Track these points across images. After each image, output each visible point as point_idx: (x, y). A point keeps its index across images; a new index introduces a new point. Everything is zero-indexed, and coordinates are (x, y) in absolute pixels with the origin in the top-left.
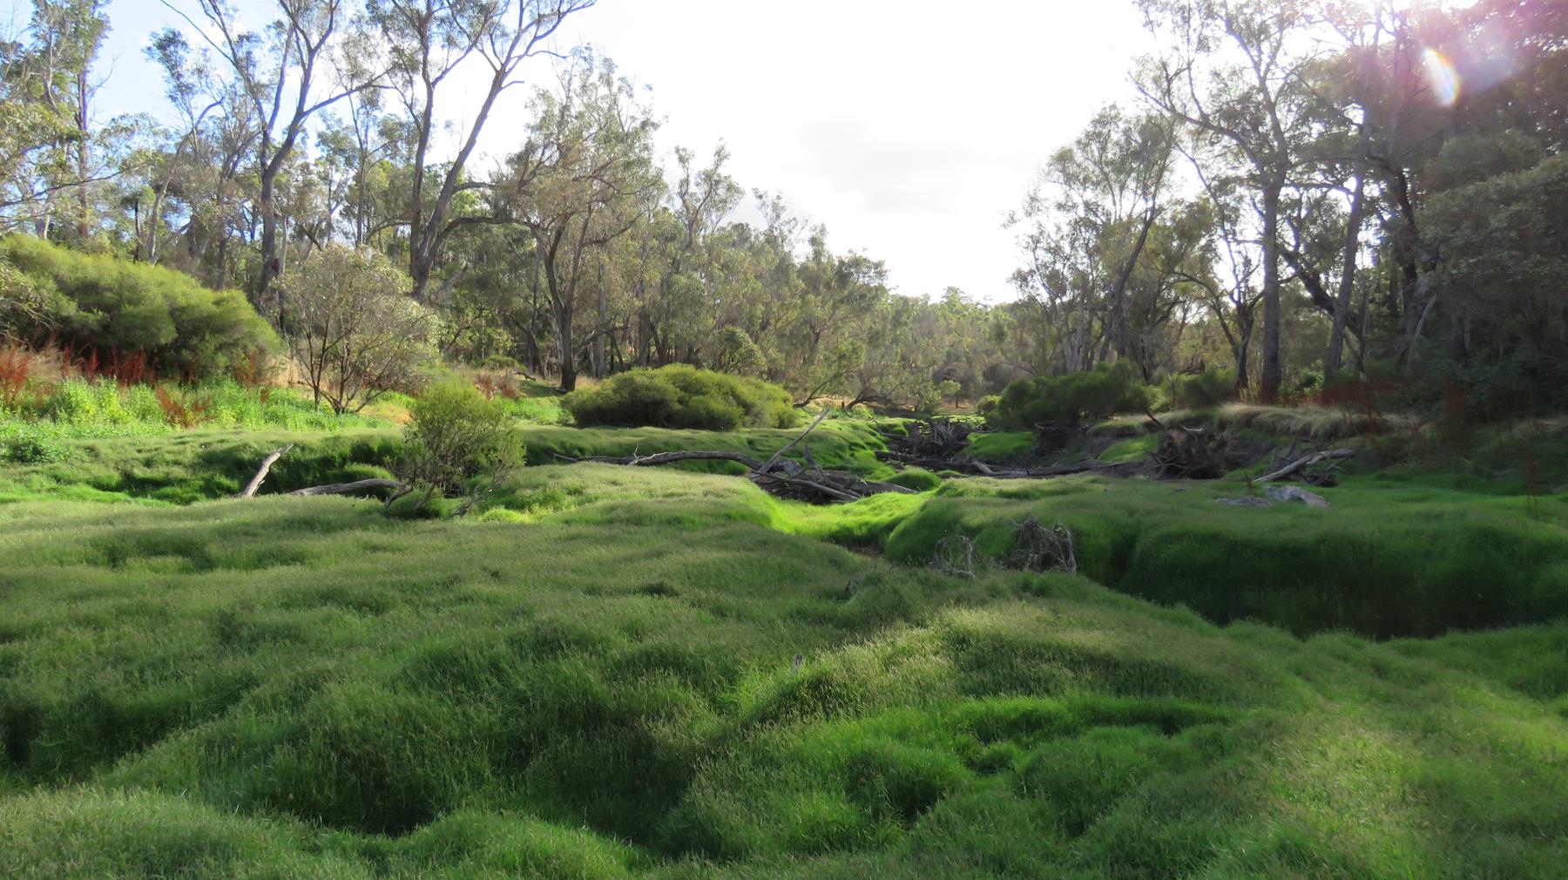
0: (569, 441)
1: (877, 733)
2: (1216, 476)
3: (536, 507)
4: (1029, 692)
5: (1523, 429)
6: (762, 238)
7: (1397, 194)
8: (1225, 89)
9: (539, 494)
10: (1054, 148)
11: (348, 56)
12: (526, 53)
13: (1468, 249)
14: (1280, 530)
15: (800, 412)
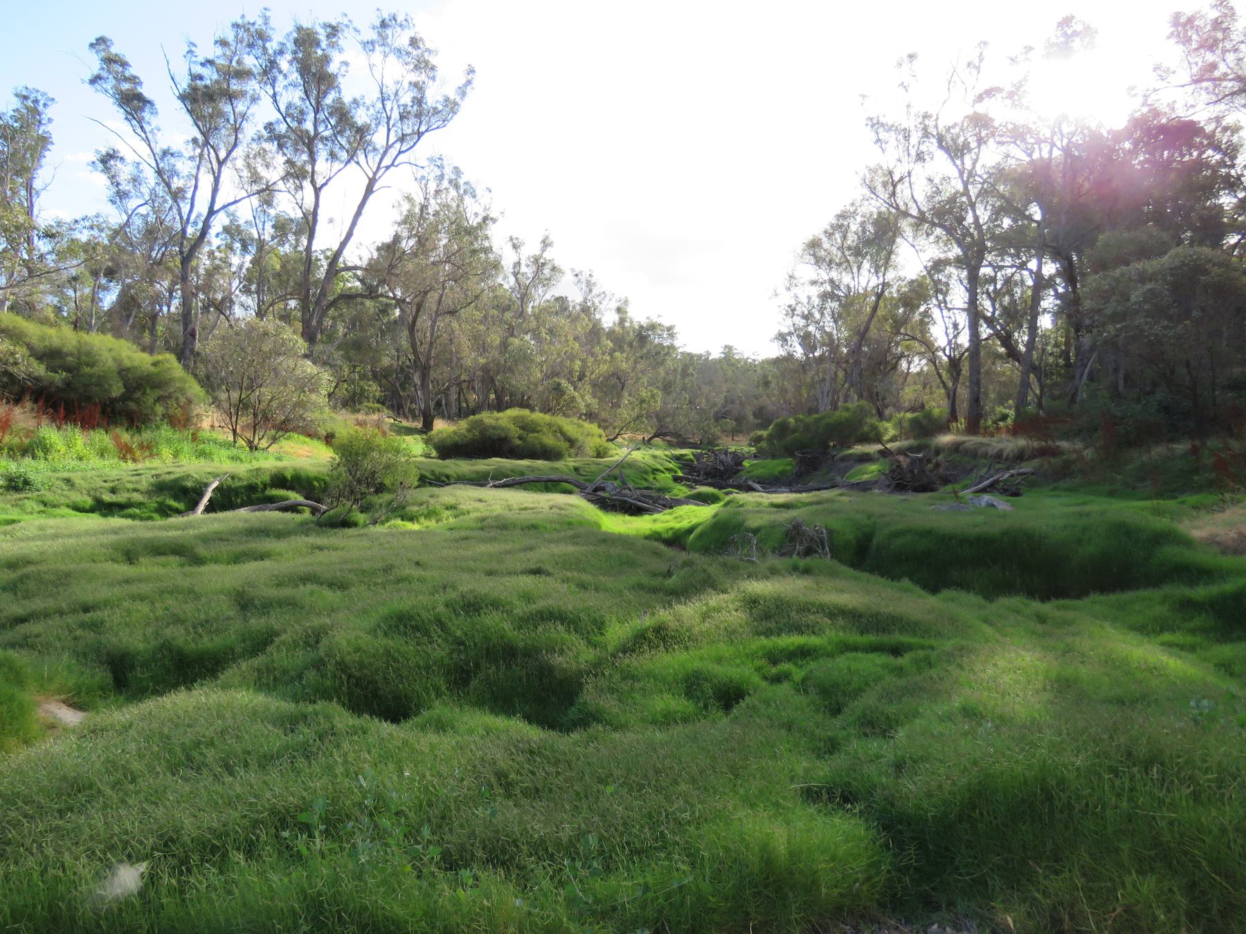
0: (437, 470)
1: (702, 659)
2: (932, 490)
3: (422, 520)
4: (801, 633)
5: (1158, 451)
6: (578, 308)
7: (1069, 274)
8: (938, 192)
9: (423, 509)
10: (808, 237)
11: (249, 166)
12: (392, 164)
13: (1115, 318)
14: (976, 526)
15: (610, 445)
